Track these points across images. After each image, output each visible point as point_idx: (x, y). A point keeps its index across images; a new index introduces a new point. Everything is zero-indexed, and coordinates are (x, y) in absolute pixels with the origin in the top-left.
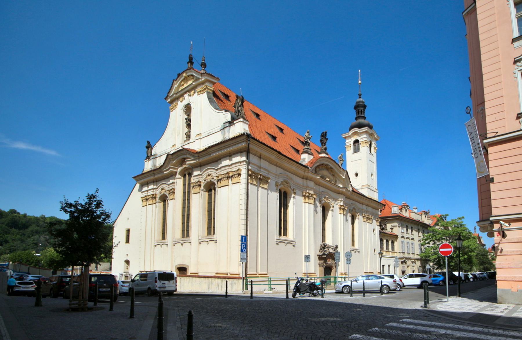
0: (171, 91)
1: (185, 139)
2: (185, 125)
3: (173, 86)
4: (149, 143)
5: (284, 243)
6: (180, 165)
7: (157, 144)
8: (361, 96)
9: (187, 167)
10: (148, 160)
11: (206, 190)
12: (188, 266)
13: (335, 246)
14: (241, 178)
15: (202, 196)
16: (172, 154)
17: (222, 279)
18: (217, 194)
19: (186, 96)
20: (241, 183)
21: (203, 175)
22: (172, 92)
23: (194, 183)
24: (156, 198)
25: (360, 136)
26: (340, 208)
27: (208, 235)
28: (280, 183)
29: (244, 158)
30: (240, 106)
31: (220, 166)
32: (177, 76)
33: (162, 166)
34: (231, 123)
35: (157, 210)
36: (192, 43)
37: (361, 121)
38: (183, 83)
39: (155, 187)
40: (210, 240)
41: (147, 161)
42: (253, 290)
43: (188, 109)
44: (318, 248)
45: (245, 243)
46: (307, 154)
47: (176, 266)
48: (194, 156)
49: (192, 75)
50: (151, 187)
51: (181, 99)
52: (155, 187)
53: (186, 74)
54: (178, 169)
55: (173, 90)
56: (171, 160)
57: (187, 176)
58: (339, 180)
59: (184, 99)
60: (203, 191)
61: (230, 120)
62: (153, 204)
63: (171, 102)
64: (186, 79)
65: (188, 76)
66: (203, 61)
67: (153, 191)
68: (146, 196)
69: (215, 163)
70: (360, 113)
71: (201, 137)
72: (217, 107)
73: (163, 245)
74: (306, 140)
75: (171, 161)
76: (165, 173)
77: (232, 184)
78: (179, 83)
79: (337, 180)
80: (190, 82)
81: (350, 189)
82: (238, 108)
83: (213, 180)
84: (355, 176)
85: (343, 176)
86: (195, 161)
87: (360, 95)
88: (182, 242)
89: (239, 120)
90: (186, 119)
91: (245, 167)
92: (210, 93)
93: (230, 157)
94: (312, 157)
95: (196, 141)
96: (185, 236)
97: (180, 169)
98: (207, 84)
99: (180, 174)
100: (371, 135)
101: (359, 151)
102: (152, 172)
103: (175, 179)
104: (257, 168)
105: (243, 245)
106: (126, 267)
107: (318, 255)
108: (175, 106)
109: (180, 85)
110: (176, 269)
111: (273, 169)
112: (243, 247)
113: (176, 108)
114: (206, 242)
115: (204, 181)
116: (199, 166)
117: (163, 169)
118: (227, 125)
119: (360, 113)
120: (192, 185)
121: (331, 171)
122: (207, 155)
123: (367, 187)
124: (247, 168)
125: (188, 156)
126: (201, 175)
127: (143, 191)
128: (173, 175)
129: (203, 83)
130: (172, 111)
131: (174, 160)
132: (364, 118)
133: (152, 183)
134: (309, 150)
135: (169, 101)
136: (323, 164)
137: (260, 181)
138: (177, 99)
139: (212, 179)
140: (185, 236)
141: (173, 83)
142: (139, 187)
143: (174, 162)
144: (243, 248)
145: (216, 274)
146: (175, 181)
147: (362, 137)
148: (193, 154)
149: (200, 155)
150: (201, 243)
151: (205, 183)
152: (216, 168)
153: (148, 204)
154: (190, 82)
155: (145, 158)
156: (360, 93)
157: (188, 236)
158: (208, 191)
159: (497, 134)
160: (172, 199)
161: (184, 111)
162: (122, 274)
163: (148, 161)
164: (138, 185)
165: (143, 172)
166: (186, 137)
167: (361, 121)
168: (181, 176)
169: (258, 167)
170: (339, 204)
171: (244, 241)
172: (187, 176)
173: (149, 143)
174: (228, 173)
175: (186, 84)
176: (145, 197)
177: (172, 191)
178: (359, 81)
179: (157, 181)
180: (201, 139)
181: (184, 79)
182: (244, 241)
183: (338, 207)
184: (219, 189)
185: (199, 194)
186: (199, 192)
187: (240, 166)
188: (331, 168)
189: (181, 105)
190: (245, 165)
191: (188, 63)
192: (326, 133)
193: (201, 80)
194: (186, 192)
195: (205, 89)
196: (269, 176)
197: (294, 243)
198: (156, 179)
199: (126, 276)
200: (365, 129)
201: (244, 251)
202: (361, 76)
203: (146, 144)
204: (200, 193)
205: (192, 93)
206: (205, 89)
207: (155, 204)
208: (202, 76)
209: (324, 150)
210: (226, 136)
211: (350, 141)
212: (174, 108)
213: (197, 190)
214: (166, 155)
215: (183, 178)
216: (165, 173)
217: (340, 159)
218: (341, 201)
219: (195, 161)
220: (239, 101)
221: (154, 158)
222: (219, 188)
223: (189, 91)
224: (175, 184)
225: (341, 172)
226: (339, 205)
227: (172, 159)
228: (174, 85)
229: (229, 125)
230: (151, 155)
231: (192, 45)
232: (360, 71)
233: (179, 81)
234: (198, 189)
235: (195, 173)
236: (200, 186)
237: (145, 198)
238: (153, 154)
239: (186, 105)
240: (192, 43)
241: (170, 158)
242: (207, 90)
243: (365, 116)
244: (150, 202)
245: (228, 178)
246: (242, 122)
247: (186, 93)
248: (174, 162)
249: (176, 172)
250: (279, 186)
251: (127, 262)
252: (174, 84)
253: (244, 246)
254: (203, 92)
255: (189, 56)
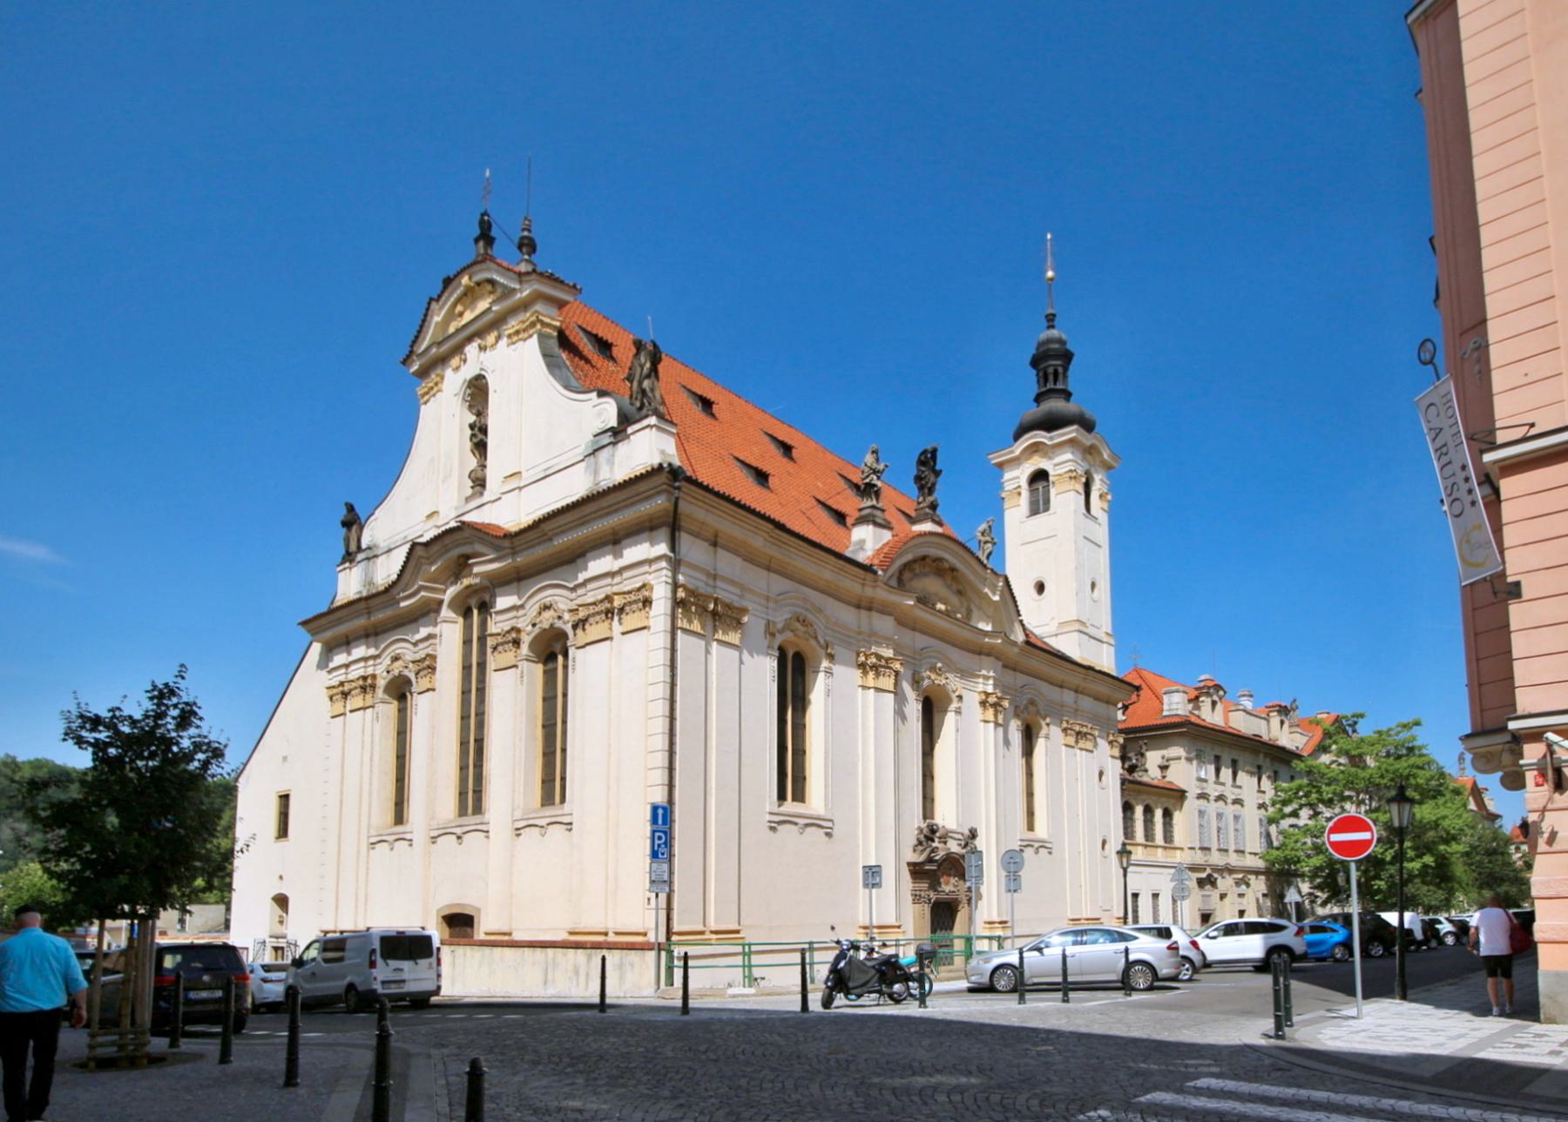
0: (422, 335)
1: (470, 492)
2: (468, 445)
3: (428, 318)
4: (350, 508)
5: (796, 824)
6: (452, 579)
7: (377, 512)
8: (1053, 320)
9: (476, 584)
10: (347, 565)
11: (538, 656)
12: (479, 910)
13: (967, 832)
14: (652, 613)
15: (525, 678)
16: (427, 545)
17: (589, 951)
18: (574, 669)
19: (471, 350)
20: (652, 631)
21: (527, 606)
22: (424, 339)
23: (499, 634)
24: (373, 687)
25: (1050, 458)
26: (983, 703)
27: (543, 805)
28: (780, 626)
29: (662, 548)
30: (648, 376)
31: (582, 577)
32: (440, 286)
33: (394, 583)
34: (618, 433)
35: (377, 727)
36: (488, 174)
37: (1055, 405)
38: (459, 308)
39: (372, 651)
40: (549, 820)
41: (345, 569)
42: (691, 986)
43: (478, 391)
44: (910, 838)
45: (665, 828)
46: (871, 527)
47: (438, 911)
48: (497, 548)
49: (491, 282)
50: (360, 651)
51: (455, 361)
52: (372, 651)
53: (470, 278)
54: (445, 591)
55: (427, 332)
56: (423, 560)
57: (475, 612)
58: (980, 608)
59: (465, 361)
60: (527, 660)
61: (615, 425)
62: (364, 708)
63: (423, 373)
64: (469, 296)
65: (478, 284)
66: (526, 233)
67: (365, 667)
68: (342, 684)
69: (565, 567)
70: (1051, 378)
71: (522, 485)
72: (574, 383)
73: (397, 843)
74: (867, 480)
75: (423, 568)
76: (403, 604)
77: (623, 634)
78: (446, 307)
79: (974, 609)
80: (483, 305)
81: (1020, 637)
82: (640, 383)
83: (559, 624)
84: (1033, 592)
85: (994, 594)
86: (504, 564)
87: (1051, 320)
88: (543, 822)
89: (645, 422)
90: (472, 427)
91: (664, 579)
92: (549, 336)
93: (618, 547)
94: (887, 536)
95: (504, 497)
96: (470, 810)
97: (452, 591)
98: (539, 307)
99: (452, 605)
100: (1090, 454)
101: (1047, 509)
102: (362, 605)
103: (435, 624)
104: (704, 578)
105: (657, 834)
106: (277, 919)
107: (909, 864)
108: (436, 384)
109: (451, 316)
110: (440, 920)
111: (759, 579)
112: (657, 842)
113: (439, 391)
114: (537, 829)
115: (530, 627)
116: (516, 579)
117: (399, 594)
118: (607, 439)
119: (1051, 378)
120: (490, 642)
121: (954, 579)
122: (539, 544)
123: (1077, 626)
124: (670, 581)
125: (479, 548)
126: (522, 607)
127: (332, 665)
128: (428, 611)
129: (525, 305)
130: (426, 403)
131: (432, 564)
132: (1067, 395)
133: (363, 640)
134: (878, 513)
135: (415, 367)
136: (924, 558)
137: (715, 620)
138: (443, 360)
139: (556, 621)
140: (470, 810)
141: (428, 309)
142: (321, 654)
143: (433, 568)
144: (659, 846)
145: (571, 933)
146: (436, 630)
147: (1058, 459)
148: (493, 540)
149: (517, 541)
150: (522, 831)
151: (387, 680)
152: (571, 585)
153: (349, 707)
154: (483, 305)
155: (340, 560)
156: (1050, 311)
157: (478, 809)
158: (543, 658)
159: (1533, 432)
160: (428, 690)
161: (464, 399)
162: (264, 942)
163: (350, 568)
164: (316, 648)
165: (332, 603)
166: (471, 484)
167: (1055, 405)
168: (455, 612)
169: (708, 574)
170: (981, 688)
171: (660, 822)
172: (475, 612)
173: (350, 508)
174: (609, 598)
175: (472, 311)
176: (339, 686)
177: (427, 663)
178: (1046, 271)
179: (376, 634)
180: (520, 488)
181: (465, 294)
182: (660, 822)
183: (977, 698)
184: (581, 650)
185: (514, 669)
186: (513, 663)
187: (650, 573)
188: (953, 569)
189: (454, 380)
190: (665, 572)
191: (476, 241)
192: (934, 452)
193: (519, 296)
194: (470, 667)
195: (533, 325)
196: (745, 604)
197: (830, 824)
198: (374, 626)
199: (276, 949)
200: (1071, 432)
201: (663, 854)
202: (1053, 254)
203: (342, 513)
204: (515, 666)
205: (491, 338)
206: (533, 325)
207: (373, 707)
208: (521, 282)
209: (927, 510)
210: (601, 478)
211: (1017, 477)
212: (432, 393)
213: (507, 657)
214: (406, 548)
215: (461, 620)
216: (403, 604)
217: (983, 539)
218: (986, 678)
219: (504, 564)
220: (643, 359)
221: (368, 559)
222: (578, 648)
223: (479, 334)
224: (437, 641)
225: (986, 579)
226: (980, 693)
227: (428, 558)
228: (432, 317)
229: (612, 439)
230: (359, 549)
231: (488, 179)
232: (1049, 236)
233: (449, 303)
234: (511, 654)
235: (503, 602)
236: (517, 643)
237: (341, 689)
238: (364, 546)
239: (470, 381)
240: (488, 174)
241: (420, 557)
242: (539, 326)
243: (1070, 389)
244: (356, 701)
245: (609, 613)
246: (654, 429)
247: (470, 339)
248: (433, 568)
249: (441, 602)
250: (777, 635)
251: (282, 901)
252: (430, 313)
253: (660, 838)
254: (526, 335)
255: (479, 217)
